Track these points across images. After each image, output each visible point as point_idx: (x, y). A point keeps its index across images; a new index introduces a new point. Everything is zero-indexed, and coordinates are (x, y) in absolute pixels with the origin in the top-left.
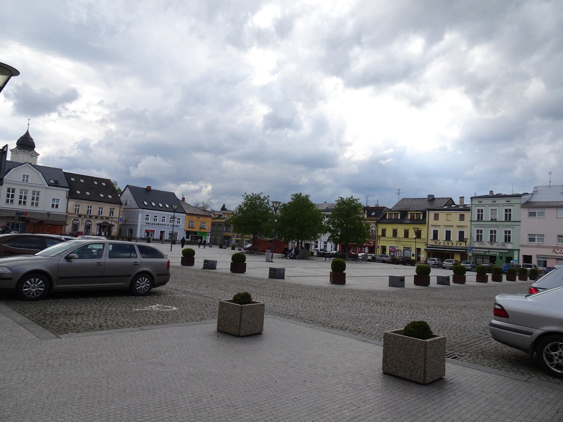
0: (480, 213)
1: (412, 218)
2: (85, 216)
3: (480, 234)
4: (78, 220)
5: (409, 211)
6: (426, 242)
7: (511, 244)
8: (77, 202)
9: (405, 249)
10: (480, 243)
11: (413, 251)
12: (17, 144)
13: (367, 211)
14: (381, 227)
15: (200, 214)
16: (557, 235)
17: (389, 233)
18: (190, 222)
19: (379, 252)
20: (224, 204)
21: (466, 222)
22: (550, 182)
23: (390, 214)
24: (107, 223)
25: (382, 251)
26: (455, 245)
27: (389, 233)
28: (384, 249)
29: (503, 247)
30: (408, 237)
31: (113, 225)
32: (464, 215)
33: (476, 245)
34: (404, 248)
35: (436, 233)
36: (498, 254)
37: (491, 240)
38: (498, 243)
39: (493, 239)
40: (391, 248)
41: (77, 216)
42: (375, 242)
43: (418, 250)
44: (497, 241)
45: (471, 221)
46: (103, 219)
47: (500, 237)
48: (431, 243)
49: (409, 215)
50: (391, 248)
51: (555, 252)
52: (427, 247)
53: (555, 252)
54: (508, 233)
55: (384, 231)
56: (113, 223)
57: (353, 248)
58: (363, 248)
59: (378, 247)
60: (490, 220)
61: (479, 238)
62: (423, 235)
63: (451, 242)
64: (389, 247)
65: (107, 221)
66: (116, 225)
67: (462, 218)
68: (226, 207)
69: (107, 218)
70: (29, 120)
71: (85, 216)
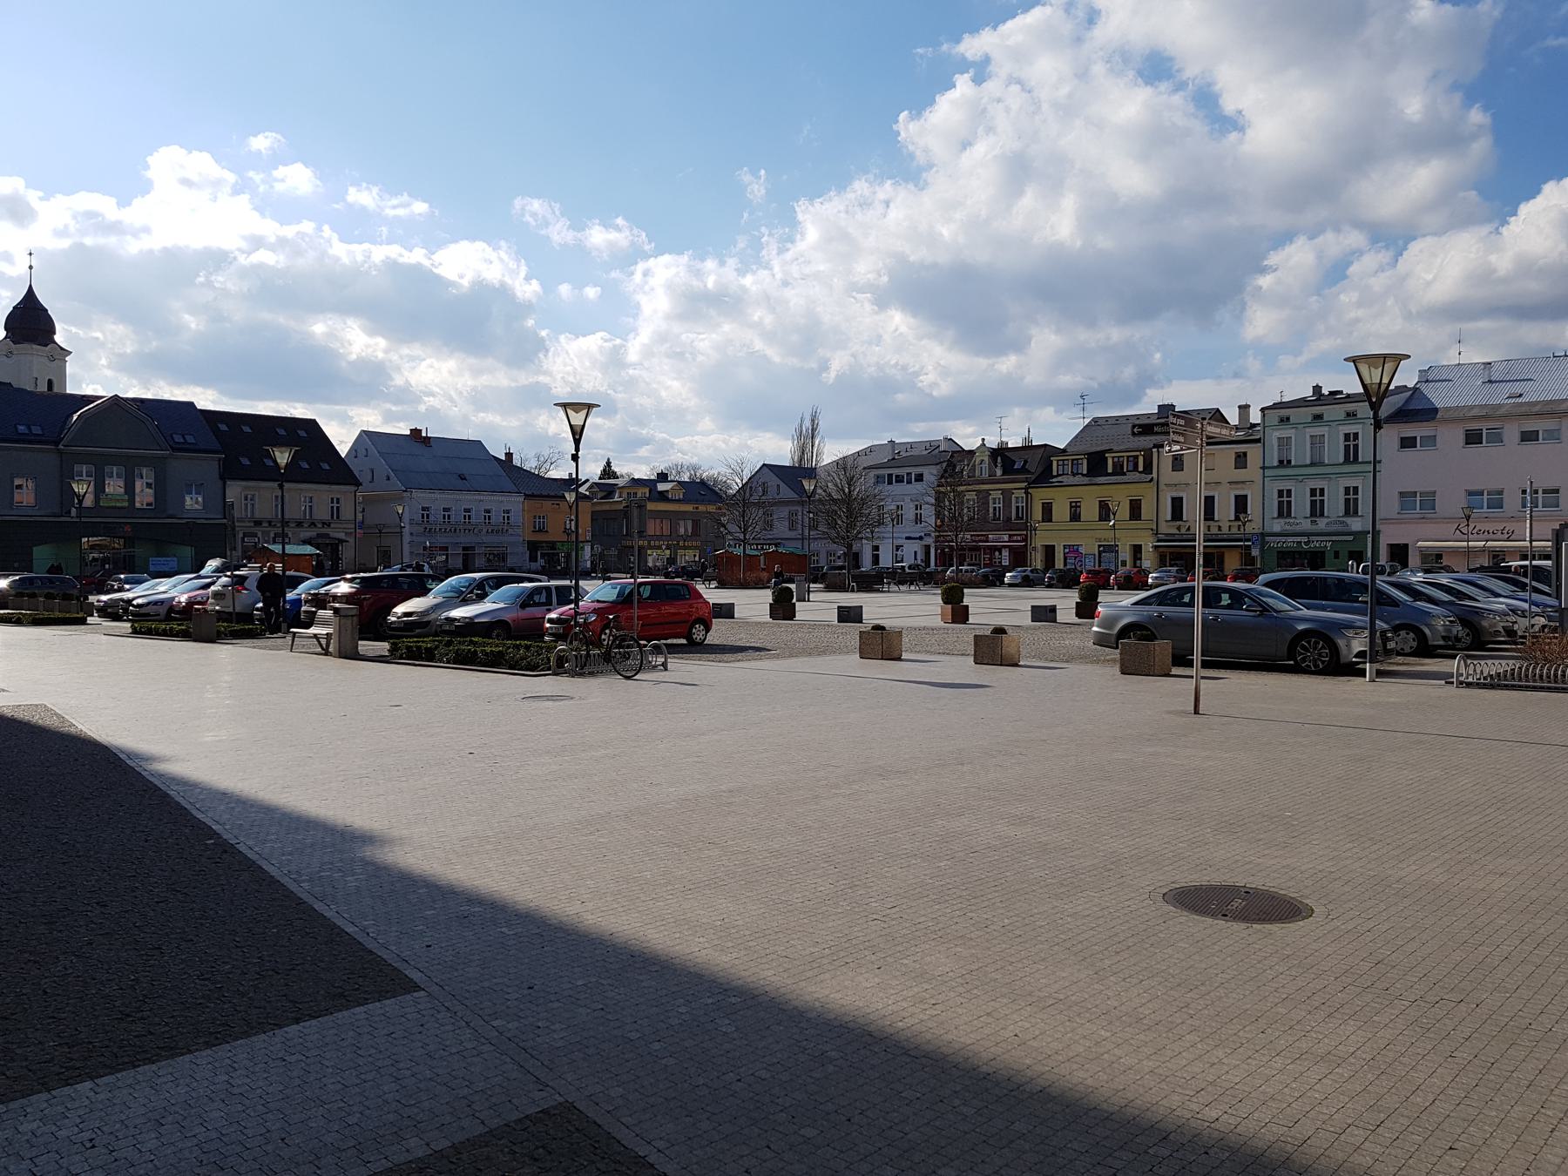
0: (335, 505)
1: (1118, 470)
2: (270, 522)
3: (1351, 496)
4: (255, 535)
5: (1110, 451)
6: (1155, 527)
7: (1359, 519)
8: (246, 488)
9: (1101, 549)
10: (1287, 520)
11: (1125, 554)
12: (6, 329)
13: (1002, 459)
14: (1040, 495)
15: (553, 494)
16: (1466, 490)
17: (1061, 511)
18: (535, 517)
19: (1038, 561)
20: (609, 459)
21: (1253, 470)
22: (1460, 354)
23: (1061, 463)
24: (327, 536)
25: (1044, 559)
26: (1225, 530)
27: (1061, 511)
28: (1049, 551)
29: (1340, 528)
30: (1050, 520)
31: (341, 541)
32: (1245, 454)
33: (1277, 526)
34: (1100, 546)
35: (1177, 504)
36: (1329, 544)
37: (1313, 514)
38: (1328, 517)
39: (1317, 510)
40: (1067, 550)
41: (252, 524)
42: (1026, 536)
43: (1137, 550)
44: (1326, 514)
45: (1263, 468)
46: (315, 526)
47: (1334, 504)
48: (1165, 529)
49: (1110, 462)
50: (1067, 550)
51: (1461, 532)
52: (1158, 541)
53: (1461, 532)
54: (1351, 493)
55: (1047, 510)
56: (342, 536)
57: (972, 556)
58: (997, 553)
59: (1034, 549)
60: (1276, 464)
61: (1284, 511)
62: (1147, 510)
63: (1217, 524)
64: (1062, 548)
65: (325, 530)
66: (351, 540)
67: (1241, 460)
68: (615, 468)
69: (326, 524)
70: (30, 254)
71: (270, 522)
